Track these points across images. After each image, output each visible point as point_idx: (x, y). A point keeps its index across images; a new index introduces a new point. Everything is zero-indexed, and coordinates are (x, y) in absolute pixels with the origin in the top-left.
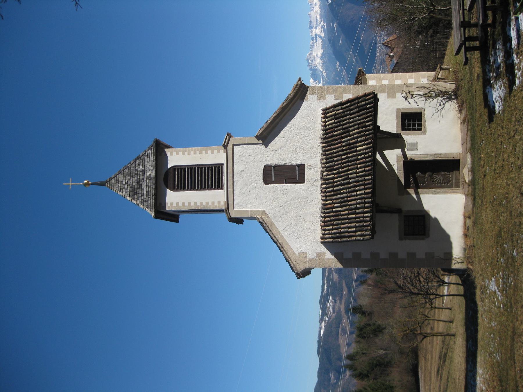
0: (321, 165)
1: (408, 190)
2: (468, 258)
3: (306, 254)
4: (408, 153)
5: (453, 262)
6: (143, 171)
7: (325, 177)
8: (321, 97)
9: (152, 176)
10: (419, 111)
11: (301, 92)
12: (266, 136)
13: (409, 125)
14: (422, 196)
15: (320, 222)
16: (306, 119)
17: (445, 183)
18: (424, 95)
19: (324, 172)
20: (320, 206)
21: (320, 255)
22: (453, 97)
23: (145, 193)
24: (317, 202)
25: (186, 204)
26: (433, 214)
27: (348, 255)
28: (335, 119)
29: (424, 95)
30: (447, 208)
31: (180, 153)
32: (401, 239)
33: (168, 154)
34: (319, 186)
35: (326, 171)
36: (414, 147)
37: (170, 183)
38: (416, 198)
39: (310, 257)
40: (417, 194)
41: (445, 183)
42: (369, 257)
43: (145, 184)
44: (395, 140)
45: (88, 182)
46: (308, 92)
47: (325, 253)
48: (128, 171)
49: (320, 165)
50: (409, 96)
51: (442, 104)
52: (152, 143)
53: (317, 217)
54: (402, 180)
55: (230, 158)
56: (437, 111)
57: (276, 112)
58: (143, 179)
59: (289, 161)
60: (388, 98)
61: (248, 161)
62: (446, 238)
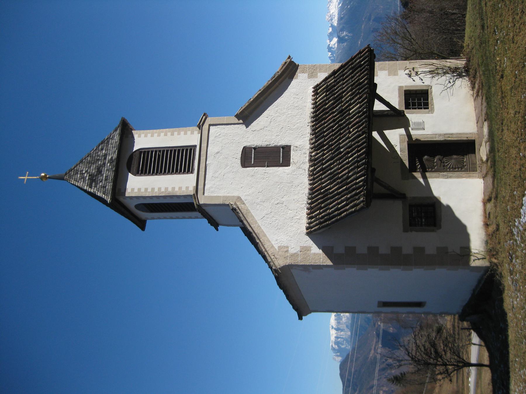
0: (309, 146)
1: (414, 174)
2: (492, 251)
3: (287, 247)
4: (412, 132)
5: (472, 258)
6: (105, 156)
7: (313, 158)
8: (312, 76)
9: (114, 158)
10: (425, 88)
11: (290, 70)
12: (248, 115)
13: (414, 104)
14: (430, 181)
15: (306, 210)
16: (294, 98)
17: (458, 168)
18: (431, 72)
19: (312, 153)
20: (307, 191)
21: (305, 249)
22: (464, 74)
23: (104, 178)
24: (304, 187)
25: (149, 190)
26: (444, 201)
27: (340, 250)
28: (327, 91)
29: (431, 72)
30: (462, 194)
31: (149, 135)
32: (405, 230)
33: (136, 137)
34: (307, 170)
35: (315, 150)
36: (421, 126)
37: (134, 167)
38: (423, 183)
39: (292, 251)
40: (425, 178)
41: (458, 168)
42: (365, 251)
43: (106, 169)
44: (395, 118)
45: (46, 175)
46: (298, 71)
47: (311, 247)
48: (92, 159)
49: (308, 146)
50: (413, 74)
51: (451, 81)
52: (118, 123)
53: (302, 204)
54: (407, 163)
55: (204, 140)
56: (446, 88)
57: (260, 90)
58: (104, 164)
59: (273, 142)
60: (389, 75)
61: (226, 141)
62: (461, 230)
